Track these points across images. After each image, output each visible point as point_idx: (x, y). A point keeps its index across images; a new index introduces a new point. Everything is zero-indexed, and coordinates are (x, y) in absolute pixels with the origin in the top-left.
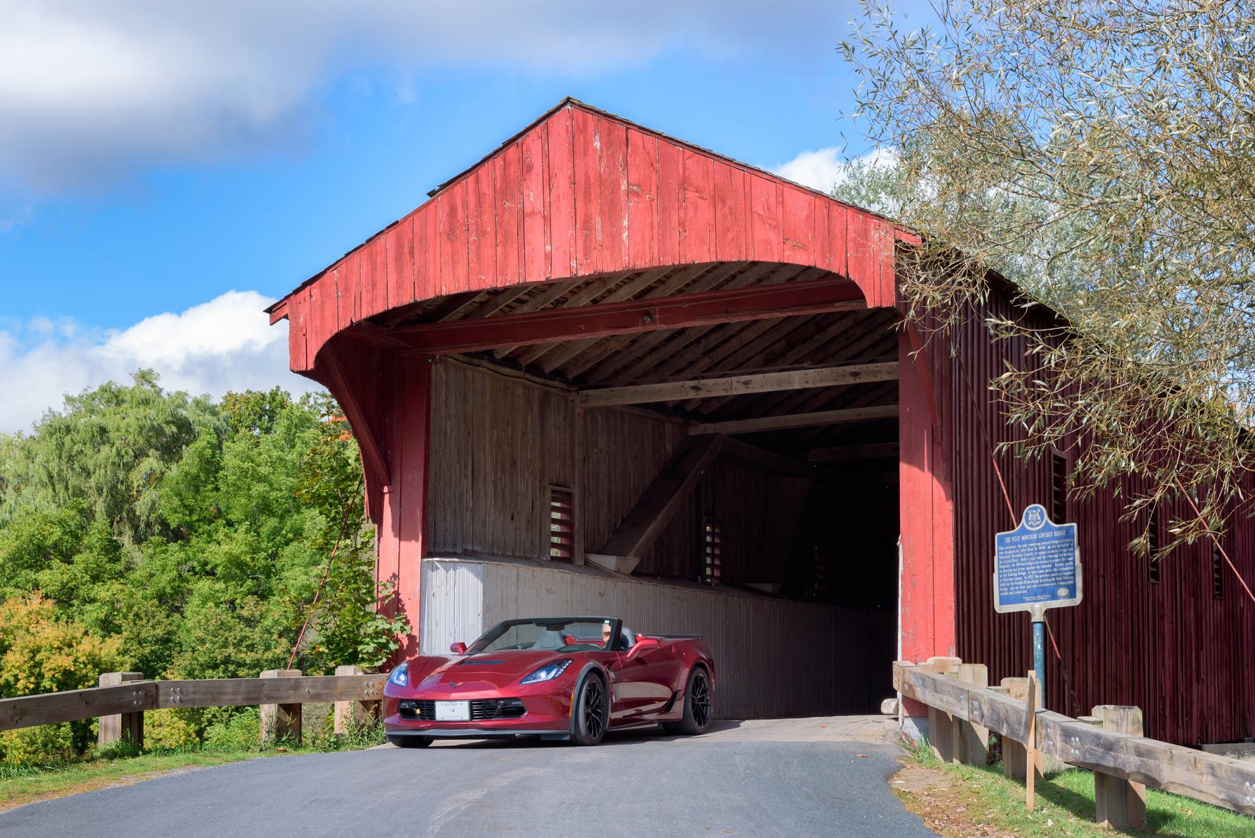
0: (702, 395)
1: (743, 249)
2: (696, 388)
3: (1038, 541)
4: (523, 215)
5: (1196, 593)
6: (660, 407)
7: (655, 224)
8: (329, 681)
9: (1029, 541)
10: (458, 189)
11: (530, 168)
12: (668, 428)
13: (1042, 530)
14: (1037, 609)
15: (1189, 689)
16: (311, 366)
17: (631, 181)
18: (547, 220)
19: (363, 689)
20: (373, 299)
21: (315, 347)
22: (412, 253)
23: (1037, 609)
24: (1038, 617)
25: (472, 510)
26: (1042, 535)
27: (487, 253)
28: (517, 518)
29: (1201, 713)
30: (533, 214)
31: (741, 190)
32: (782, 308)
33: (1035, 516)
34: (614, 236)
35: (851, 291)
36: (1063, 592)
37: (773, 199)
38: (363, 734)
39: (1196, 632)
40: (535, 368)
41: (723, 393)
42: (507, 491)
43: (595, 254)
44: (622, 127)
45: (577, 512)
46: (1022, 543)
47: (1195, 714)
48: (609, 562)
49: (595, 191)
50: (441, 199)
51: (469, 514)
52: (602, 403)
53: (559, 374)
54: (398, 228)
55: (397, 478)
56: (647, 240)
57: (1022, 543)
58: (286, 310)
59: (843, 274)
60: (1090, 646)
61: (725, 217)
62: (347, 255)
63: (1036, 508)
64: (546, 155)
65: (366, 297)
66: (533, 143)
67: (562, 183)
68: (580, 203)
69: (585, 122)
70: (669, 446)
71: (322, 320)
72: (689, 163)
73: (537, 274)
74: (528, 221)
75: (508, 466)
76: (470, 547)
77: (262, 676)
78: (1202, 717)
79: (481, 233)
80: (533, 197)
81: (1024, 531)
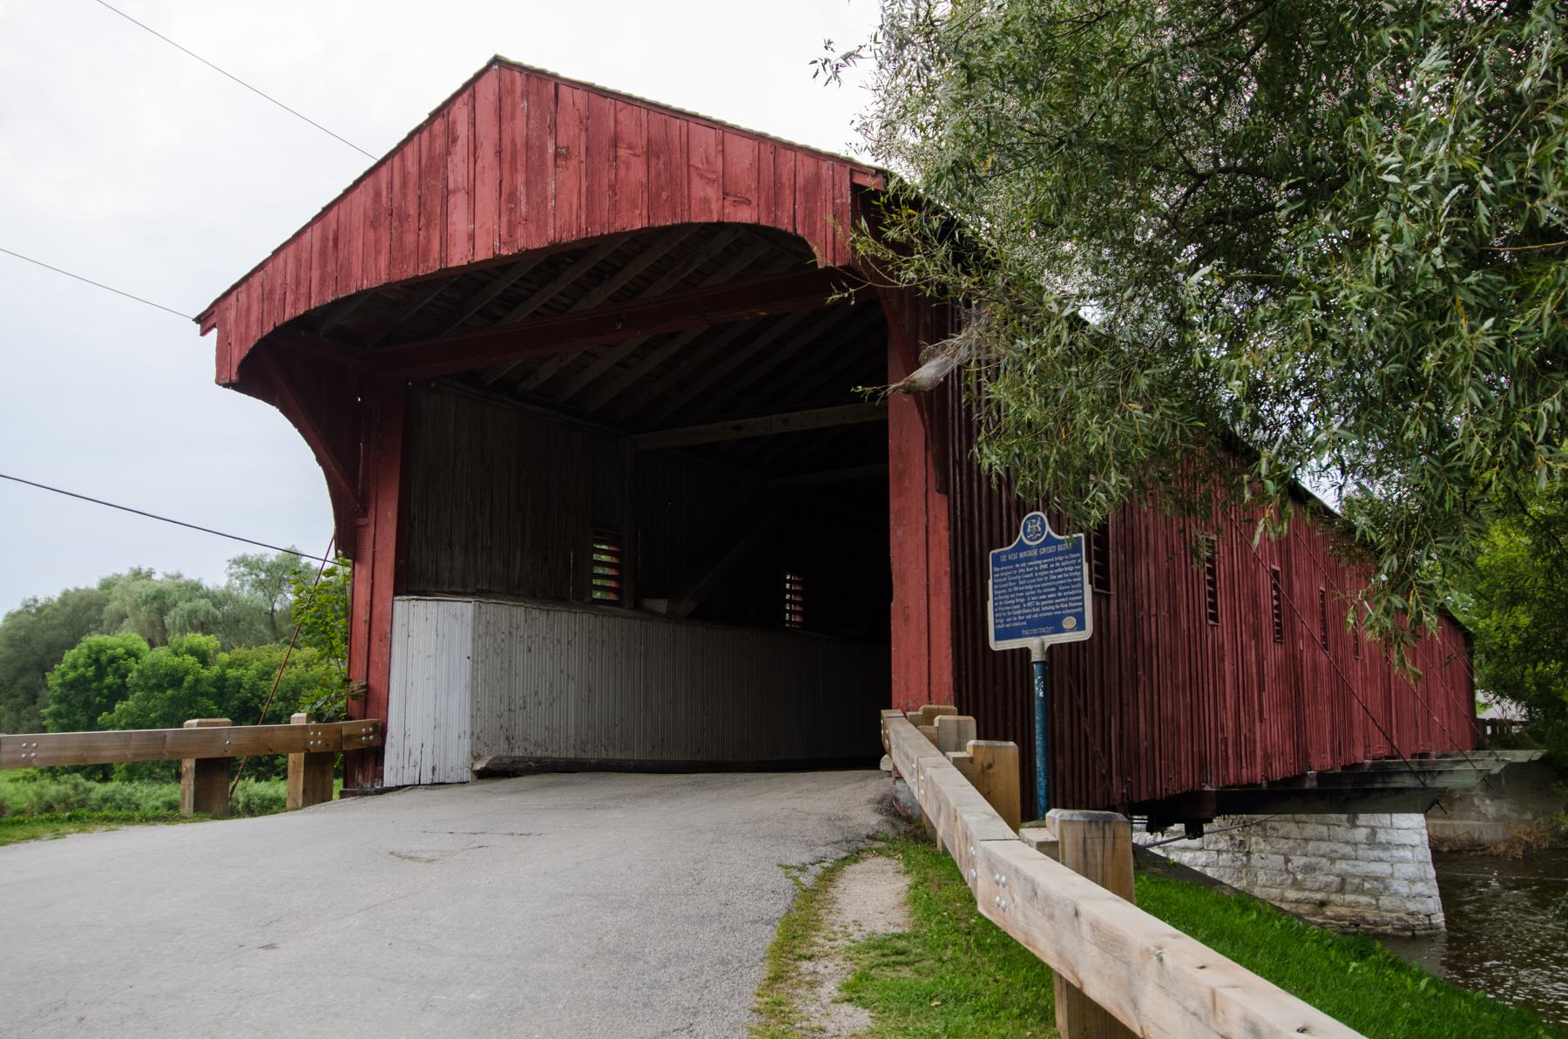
3: (1040, 557)
4: (447, 194)
5: (1256, 634)
7: (584, 189)
11: (455, 140)
13: (1044, 544)
14: (1035, 645)
15: (1252, 730)
16: (234, 378)
18: (471, 194)
20: (296, 300)
22: (336, 245)
24: (1036, 656)
26: (1043, 550)
27: (410, 239)
29: (1265, 751)
36: (1070, 622)
37: (712, 150)
39: (1258, 673)
43: (520, 232)
46: (1019, 561)
47: (1259, 753)
48: (661, 606)
55: (372, 511)
57: (1019, 561)
58: (213, 320)
59: (790, 230)
61: (658, 175)
63: (1035, 517)
65: (290, 298)
69: (513, 81)
71: (247, 327)
72: (621, 116)
74: (452, 200)
81: (1022, 547)
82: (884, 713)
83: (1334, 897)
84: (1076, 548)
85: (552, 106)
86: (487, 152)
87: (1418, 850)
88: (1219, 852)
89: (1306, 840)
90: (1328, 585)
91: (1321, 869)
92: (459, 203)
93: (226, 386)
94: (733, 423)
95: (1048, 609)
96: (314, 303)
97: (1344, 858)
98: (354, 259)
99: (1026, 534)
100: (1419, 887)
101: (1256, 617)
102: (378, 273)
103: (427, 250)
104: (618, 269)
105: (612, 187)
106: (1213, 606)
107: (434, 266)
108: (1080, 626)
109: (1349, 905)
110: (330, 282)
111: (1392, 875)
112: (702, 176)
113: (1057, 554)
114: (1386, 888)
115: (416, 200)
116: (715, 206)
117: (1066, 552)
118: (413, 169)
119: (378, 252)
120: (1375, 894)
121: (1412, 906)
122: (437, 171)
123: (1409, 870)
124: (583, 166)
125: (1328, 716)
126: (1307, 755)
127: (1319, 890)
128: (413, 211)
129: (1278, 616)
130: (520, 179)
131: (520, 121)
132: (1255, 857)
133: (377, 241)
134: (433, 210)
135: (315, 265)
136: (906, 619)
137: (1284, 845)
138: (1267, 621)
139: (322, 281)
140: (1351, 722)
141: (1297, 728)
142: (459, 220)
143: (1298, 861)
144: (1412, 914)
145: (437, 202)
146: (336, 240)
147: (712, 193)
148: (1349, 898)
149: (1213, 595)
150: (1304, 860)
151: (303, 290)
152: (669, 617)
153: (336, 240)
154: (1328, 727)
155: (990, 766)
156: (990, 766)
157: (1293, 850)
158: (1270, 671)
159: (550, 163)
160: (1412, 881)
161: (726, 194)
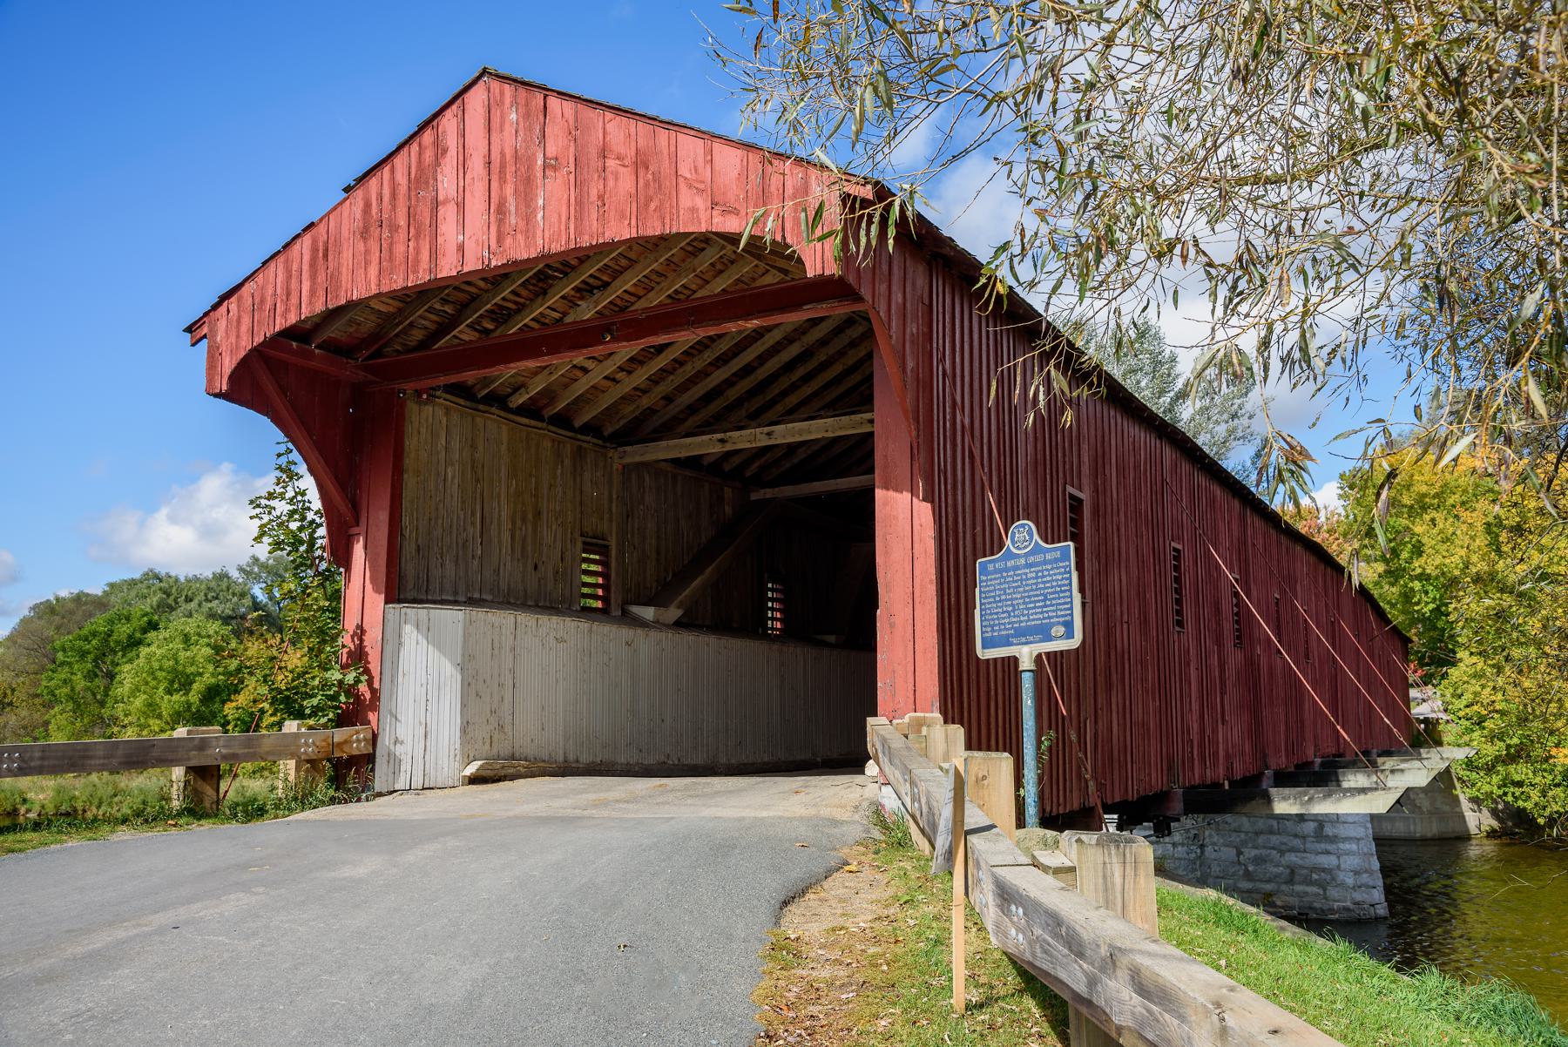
0: (729, 447)
1: (667, 221)
2: (722, 441)
4: (436, 204)
5: (1219, 641)
6: (693, 462)
8: (250, 739)
9: (1016, 568)
10: (373, 182)
11: (445, 151)
12: (728, 492)
14: (1026, 655)
15: (1215, 731)
16: (225, 388)
17: (549, 154)
18: (461, 206)
19: (299, 747)
20: (287, 310)
21: (228, 364)
22: (326, 256)
23: (1026, 655)
24: (1026, 664)
25: (481, 558)
27: (400, 249)
28: (541, 568)
30: (446, 201)
31: (665, 151)
32: (748, 316)
33: (1023, 536)
34: (529, 219)
35: (779, 255)
37: (700, 160)
38: (302, 799)
40: (562, 420)
41: (748, 445)
42: (529, 540)
43: (508, 241)
44: (539, 97)
45: (613, 564)
46: (1007, 570)
48: (648, 613)
49: (510, 169)
50: (359, 194)
51: (476, 562)
52: (638, 459)
53: (591, 429)
54: (314, 231)
55: (363, 520)
56: (564, 218)
57: (1007, 570)
60: (1114, 693)
61: (647, 185)
62: (264, 263)
63: (1023, 526)
64: (462, 134)
66: (449, 122)
67: (476, 165)
68: (495, 185)
69: (502, 93)
70: (728, 509)
71: (238, 336)
73: (448, 268)
75: (530, 516)
76: (477, 595)
77: (285, 730)
78: (1227, 756)
79: (394, 228)
80: (447, 183)
82: (870, 721)
83: (1284, 887)
84: (1065, 557)
85: (541, 118)
86: (476, 165)
87: (1362, 843)
88: (1174, 845)
89: (1257, 834)
90: (1283, 592)
91: (1272, 861)
92: (448, 214)
93: (216, 395)
94: (719, 436)
95: (1035, 619)
96: (305, 313)
97: (1293, 850)
98: (344, 270)
99: (1013, 542)
100: (1365, 878)
101: (1219, 623)
102: (368, 283)
103: (417, 261)
104: (606, 285)
105: (601, 197)
106: (1179, 613)
107: (423, 277)
108: (1069, 634)
109: (1298, 895)
110: (322, 293)
111: (1339, 867)
112: (690, 186)
113: (1045, 562)
114: (1333, 879)
115: (405, 210)
116: (704, 216)
117: (1056, 560)
118: (401, 178)
119: (367, 263)
120: (1322, 885)
121: (1358, 896)
122: (427, 183)
123: (1351, 862)
124: (572, 177)
125: (1282, 717)
126: (1265, 756)
127: (1269, 881)
128: (403, 223)
129: (1237, 622)
130: (509, 190)
131: (509, 131)
132: (1209, 849)
133: (367, 252)
134: (424, 225)
135: (305, 275)
136: (892, 626)
137: (1236, 838)
138: (1228, 626)
139: (313, 292)
140: (1302, 722)
141: (1256, 730)
142: (449, 232)
143: (1250, 853)
144: (1357, 903)
145: (427, 214)
146: (326, 251)
147: (701, 203)
148: (1298, 888)
149: (1179, 602)
150: (1254, 852)
151: (294, 300)
152: (657, 625)
153: (326, 251)
154: (1283, 728)
155: (984, 778)
156: (984, 778)
157: (1244, 843)
158: (1231, 673)
159: (539, 174)
160: (1356, 873)
161: (714, 204)
